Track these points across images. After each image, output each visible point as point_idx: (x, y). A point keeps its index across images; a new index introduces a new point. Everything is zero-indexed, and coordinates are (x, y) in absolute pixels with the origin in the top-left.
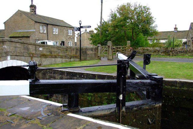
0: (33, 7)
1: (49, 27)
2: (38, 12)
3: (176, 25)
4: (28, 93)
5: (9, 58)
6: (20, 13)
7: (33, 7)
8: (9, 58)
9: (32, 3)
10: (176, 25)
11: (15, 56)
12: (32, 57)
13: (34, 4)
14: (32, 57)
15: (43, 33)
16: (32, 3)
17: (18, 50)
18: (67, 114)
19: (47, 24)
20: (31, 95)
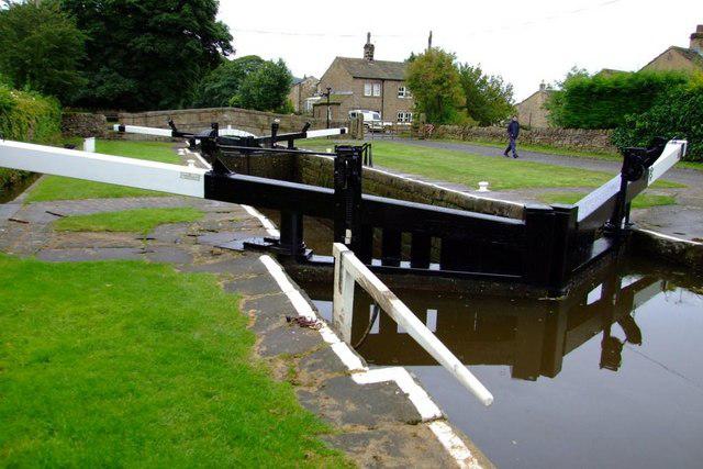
0: (369, 48)
1: (387, 84)
2: (377, 56)
3: (369, 35)
4: (201, 194)
5: (229, 126)
6: (340, 62)
7: (369, 48)
8: (229, 126)
9: (369, 40)
10: (369, 35)
11: (237, 126)
12: (262, 130)
13: (372, 42)
14: (262, 130)
15: (372, 97)
16: (369, 40)
17: (242, 120)
18: (589, 254)
19: (383, 80)
20: (208, 196)
